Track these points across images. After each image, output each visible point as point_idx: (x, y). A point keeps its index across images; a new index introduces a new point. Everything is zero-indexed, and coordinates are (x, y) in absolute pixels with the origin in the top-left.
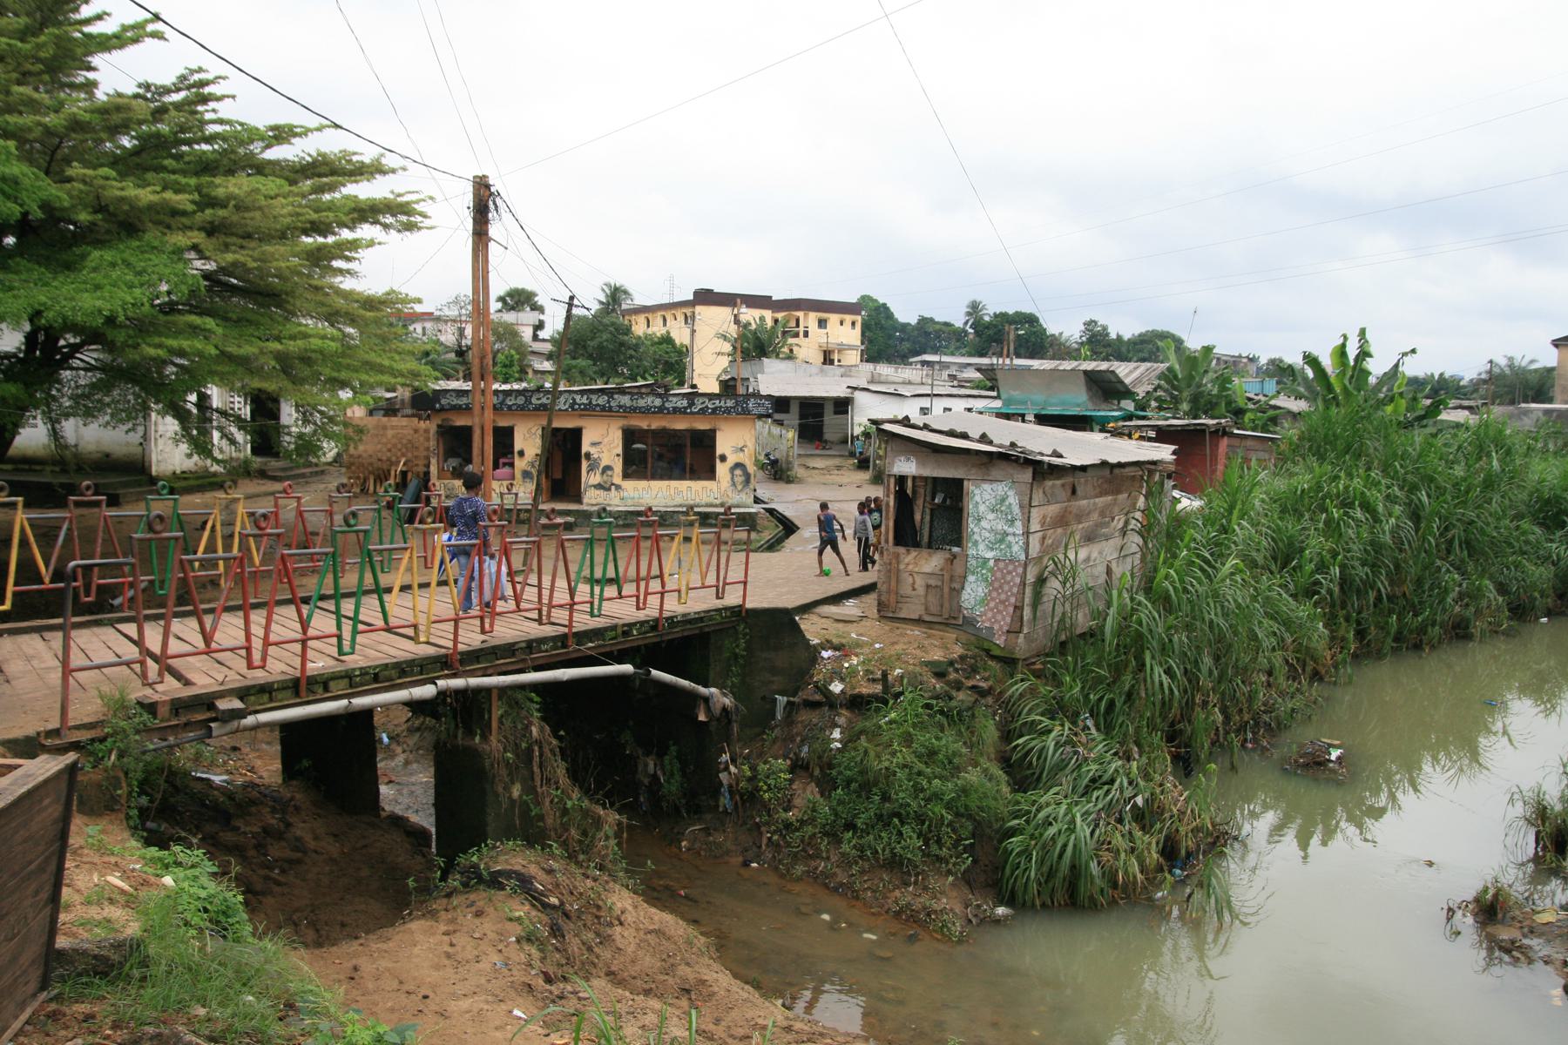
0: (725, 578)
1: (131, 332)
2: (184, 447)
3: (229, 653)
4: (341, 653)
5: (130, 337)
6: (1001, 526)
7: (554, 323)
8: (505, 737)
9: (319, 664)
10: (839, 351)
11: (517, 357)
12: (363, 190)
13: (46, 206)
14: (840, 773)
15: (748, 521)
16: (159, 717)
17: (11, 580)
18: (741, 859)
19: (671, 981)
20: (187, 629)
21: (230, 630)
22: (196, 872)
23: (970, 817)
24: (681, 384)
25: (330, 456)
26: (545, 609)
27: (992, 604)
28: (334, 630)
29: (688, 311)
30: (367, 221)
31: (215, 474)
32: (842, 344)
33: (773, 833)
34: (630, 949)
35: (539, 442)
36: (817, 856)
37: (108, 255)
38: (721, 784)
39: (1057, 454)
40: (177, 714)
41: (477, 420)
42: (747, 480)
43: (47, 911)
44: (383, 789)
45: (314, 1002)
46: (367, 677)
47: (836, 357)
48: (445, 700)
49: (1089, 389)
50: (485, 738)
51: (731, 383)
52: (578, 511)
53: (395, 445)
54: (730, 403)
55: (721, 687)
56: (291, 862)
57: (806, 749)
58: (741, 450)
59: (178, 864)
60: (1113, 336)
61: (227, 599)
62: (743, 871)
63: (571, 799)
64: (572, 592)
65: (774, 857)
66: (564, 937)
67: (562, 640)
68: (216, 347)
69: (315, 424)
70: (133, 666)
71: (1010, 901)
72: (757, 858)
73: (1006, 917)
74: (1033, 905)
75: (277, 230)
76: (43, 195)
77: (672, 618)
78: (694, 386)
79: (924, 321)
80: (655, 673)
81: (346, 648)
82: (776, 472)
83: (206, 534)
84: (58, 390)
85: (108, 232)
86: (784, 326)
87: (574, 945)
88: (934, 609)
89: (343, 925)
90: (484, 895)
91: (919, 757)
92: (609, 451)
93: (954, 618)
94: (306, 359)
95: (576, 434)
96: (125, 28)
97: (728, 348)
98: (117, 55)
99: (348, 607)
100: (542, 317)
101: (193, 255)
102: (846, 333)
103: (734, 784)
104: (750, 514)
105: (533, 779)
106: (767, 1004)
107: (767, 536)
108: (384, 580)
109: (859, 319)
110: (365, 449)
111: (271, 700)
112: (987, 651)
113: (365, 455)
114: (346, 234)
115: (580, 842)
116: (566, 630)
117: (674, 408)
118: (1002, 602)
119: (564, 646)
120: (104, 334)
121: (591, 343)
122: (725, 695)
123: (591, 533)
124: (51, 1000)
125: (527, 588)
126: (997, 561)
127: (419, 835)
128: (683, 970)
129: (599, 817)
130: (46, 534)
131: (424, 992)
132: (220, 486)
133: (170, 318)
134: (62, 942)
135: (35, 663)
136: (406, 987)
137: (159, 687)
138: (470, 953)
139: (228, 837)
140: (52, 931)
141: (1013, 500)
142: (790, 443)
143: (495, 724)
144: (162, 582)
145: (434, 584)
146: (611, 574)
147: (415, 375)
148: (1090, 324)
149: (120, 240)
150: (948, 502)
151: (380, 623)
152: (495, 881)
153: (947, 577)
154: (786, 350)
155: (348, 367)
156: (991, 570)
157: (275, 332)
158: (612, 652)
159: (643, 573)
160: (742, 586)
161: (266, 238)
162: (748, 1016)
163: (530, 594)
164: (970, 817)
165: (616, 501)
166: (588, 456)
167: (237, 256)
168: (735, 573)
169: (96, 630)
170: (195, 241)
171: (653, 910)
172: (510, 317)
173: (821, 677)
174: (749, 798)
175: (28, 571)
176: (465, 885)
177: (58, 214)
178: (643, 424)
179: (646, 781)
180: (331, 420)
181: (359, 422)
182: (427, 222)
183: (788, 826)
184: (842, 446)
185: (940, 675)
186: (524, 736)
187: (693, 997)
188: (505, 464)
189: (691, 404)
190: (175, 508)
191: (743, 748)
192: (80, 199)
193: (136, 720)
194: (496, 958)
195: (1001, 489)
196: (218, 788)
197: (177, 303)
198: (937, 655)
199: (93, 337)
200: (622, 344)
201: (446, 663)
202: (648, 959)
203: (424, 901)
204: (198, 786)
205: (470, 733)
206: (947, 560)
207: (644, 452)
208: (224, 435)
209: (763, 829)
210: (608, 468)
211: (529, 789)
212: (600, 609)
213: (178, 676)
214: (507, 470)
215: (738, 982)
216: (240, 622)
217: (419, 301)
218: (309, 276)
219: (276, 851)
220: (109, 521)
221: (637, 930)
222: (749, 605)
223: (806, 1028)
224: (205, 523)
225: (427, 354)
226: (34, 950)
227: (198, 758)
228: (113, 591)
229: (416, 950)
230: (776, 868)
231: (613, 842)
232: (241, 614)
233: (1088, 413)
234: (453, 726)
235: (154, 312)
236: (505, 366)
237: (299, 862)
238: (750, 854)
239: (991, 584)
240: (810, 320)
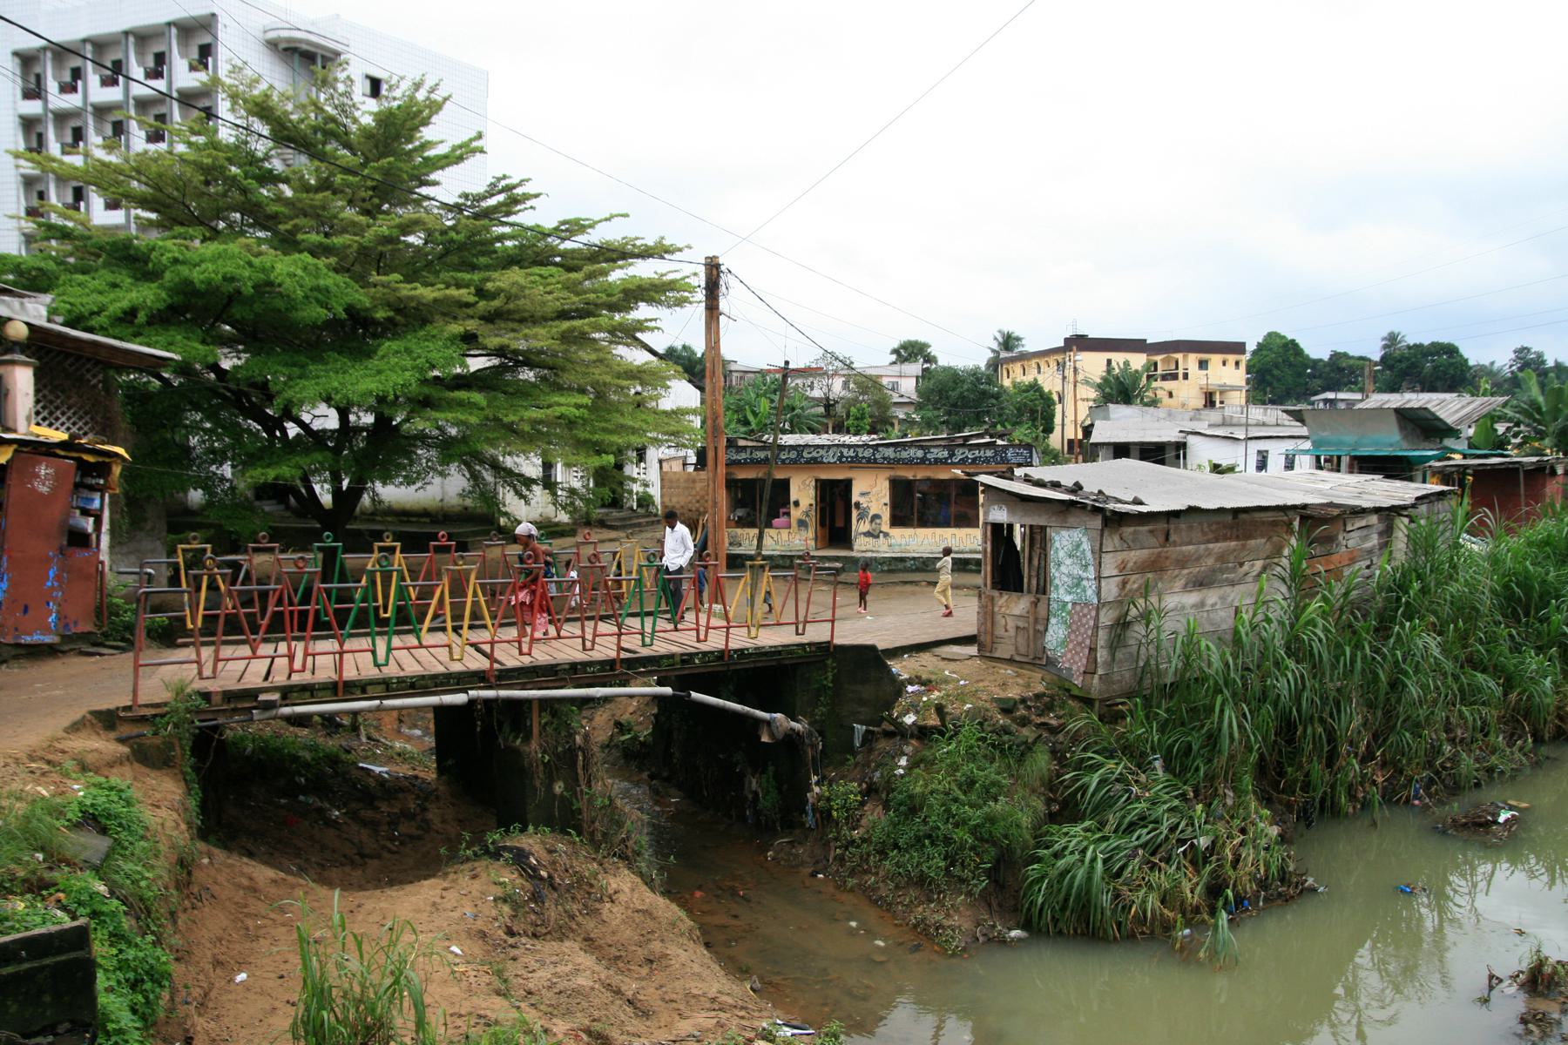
6: (1077, 571)
10: (1222, 393)
12: (644, 270)
13: (349, 309)
17: (202, 606)
23: (994, 843)
27: (1071, 646)
29: (1060, 358)
32: (1225, 385)
35: (812, 492)
39: (1138, 502)
40: (229, 702)
47: (1217, 398)
49: (1402, 428)
50: (527, 739)
52: (845, 557)
56: (412, 837)
57: (878, 774)
60: (1550, 363)
62: (808, 881)
71: (1026, 925)
73: (1020, 940)
74: (1115, 938)
76: (348, 299)
79: (1336, 356)
80: (694, 695)
88: (1023, 650)
91: (960, 786)
95: (847, 485)
96: (454, 149)
98: (450, 170)
102: (1230, 375)
111: (312, 696)
112: (1068, 690)
113: (678, 506)
117: (936, 459)
118: (1079, 644)
126: (1074, 604)
139: (368, 814)
141: (1086, 546)
143: (536, 730)
148: (1522, 352)
154: (1150, 394)
155: (604, 430)
156: (1069, 613)
164: (994, 843)
165: (885, 548)
166: (858, 505)
178: (909, 474)
179: (750, 796)
185: (1007, 711)
188: (784, 514)
189: (952, 455)
195: (1076, 535)
198: (1013, 693)
206: (1032, 603)
210: (876, 517)
216: (370, 641)
219: (405, 828)
222: (837, 641)
233: (1400, 454)
236: (857, 419)
237: (419, 838)
238: (820, 866)
239: (1070, 627)
240: (1192, 360)
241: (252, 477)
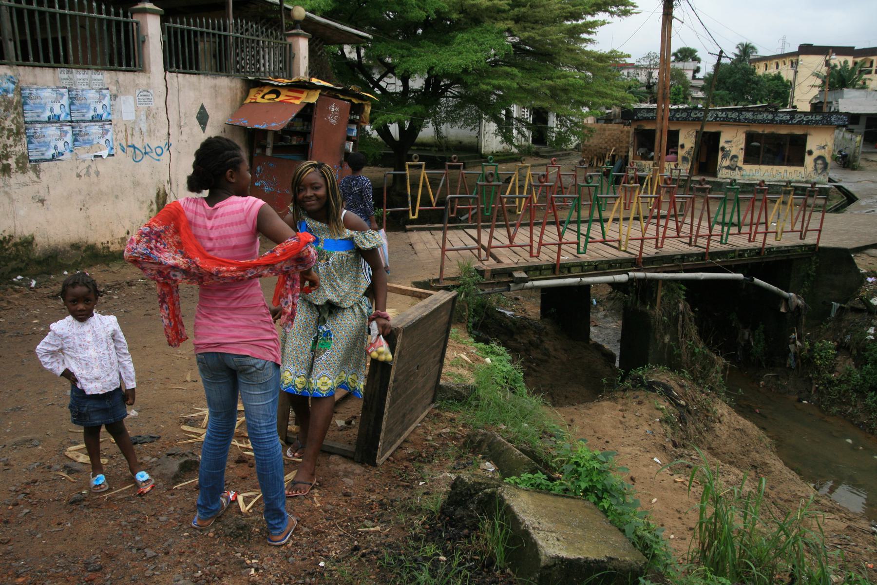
0: (807, 227)
1: (475, 77)
2: (499, 138)
3: (519, 248)
4: (578, 253)
5: (475, 80)
7: (707, 67)
8: (664, 308)
9: (565, 258)
11: (682, 89)
14: (872, 355)
15: (823, 192)
16: (485, 277)
18: (797, 397)
19: (746, 459)
20: (501, 235)
21: (522, 236)
22: (502, 358)
24: (785, 106)
25: (573, 146)
26: (693, 238)
28: (575, 240)
29: (794, 59)
30: (601, 10)
31: (513, 154)
33: (820, 385)
34: (724, 437)
35: (693, 139)
36: (848, 403)
37: (466, 36)
38: (789, 351)
40: (494, 277)
41: (659, 126)
42: (825, 165)
43: (437, 367)
44: (592, 329)
45: (563, 432)
46: (591, 267)
48: (632, 284)
50: (652, 307)
51: (819, 105)
52: (714, 182)
53: (609, 140)
54: (819, 118)
55: (796, 293)
57: (849, 337)
59: (493, 353)
61: (521, 220)
63: (698, 347)
64: (711, 229)
65: (819, 399)
66: (686, 423)
67: (702, 256)
68: (518, 84)
69: (567, 127)
70: (473, 251)
72: (807, 399)
75: (551, 18)
77: (770, 248)
78: (795, 107)
80: (756, 280)
81: (582, 250)
82: (845, 163)
83: (511, 185)
84: (439, 108)
85: (466, 23)
86: (861, 67)
87: (691, 429)
89: (566, 397)
90: (643, 393)
92: (736, 146)
94: (565, 90)
95: (717, 136)
97: (819, 82)
99: (584, 228)
100: (699, 65)
101: (507, 34)
103: (798, 352)
104: (825, 188)
105: (677, 334)
106: (804, 485)
107: (834, 203)
108: (605, 215)
110: (594, 141)
111: (540, 275)
114: (589, 18)
115: (701, 372)
116: (705, 250)
117: (781, 121)
119: (703, 260)
120: (462, 79)
122: (799, 298)
123: (726, 194)
124: (436, 408)
125: (684, 225)
127: (610, 357)
128: (754, 455)
129: (714, 360)
130: (434, 182)
131: (606, 439)
132: (516, 160)
133: (494, 68)
134: (442, 382)
135: (428, 245)
136: (597, 435)
137: (486, 263)
138: (633, 423)
139: (512, 343)
140: (439, 377)
142: (857, 144)
143: (658, 300)
144: (487, 209)
145: (631, 218)
146: (735, 219)
147: (623, 99)
149: (472, 27)
151: (600, 238)
152: (650, 387)
154: (860, 83)
155: (587, 94)
157: (549, 75)
158: (731, 266)
159: (755, 221)
160: (817, 233)
161: (545, 22)
162: (793, 488)
163: (686, 229)
166: (723, 149)
167: (530, 34)
168: (814, 224)
169: (456, 231)
170: (509, 26)
171: (740, 418)
172: (679, 65)
173: (865, 293)
174: (807, 362)
175: (426, 201)
176: (634, 386)
177: (442, 15)
178: (759, 130)
179: (743, 343)
180: (576, 124)
181: (590, 126)
182: (636, 10)
183: (830, 382)
186: (675, 308)
187: (759, 471)
188: (672, 153)
189: (792, 118)
190: (496, 170)
191: (807, 331)
192: (453, 7)
193: (475, 278)
194: (647, 428)
196: (508, 318)
197: (499, 61)
199: (456, 79)
200: (749, 80)
201: (635, 263)
202: (733, 444)
203: (611, 392)
204: (499, 316)
205: (644, 303)
207: (758, 148)
208: (519, 132)
209: (814, 381)
210: (735, 157)
211: (674, 338)
212: (726, 240)
213: (495, 258)
214: (673, 156)
215: (787, 468)
217: (629, 56)
218: (568, 44)
219: (535, 354)
220: (464, 175)
221: (729, 427)
222: (821, 245)
223: (828, 504)
224: (510, 178)
225: (630, 88)
226: (431, 384)
227: (498, 302)
228: (461, 212)
229: (604, 417)
230: (820, 406)
231: (720, 375)
232: (528, 228)
234: (635, 298)
235: (487, 65)
236: (675, 94)
237: (546, 361)
241: (381, 120)
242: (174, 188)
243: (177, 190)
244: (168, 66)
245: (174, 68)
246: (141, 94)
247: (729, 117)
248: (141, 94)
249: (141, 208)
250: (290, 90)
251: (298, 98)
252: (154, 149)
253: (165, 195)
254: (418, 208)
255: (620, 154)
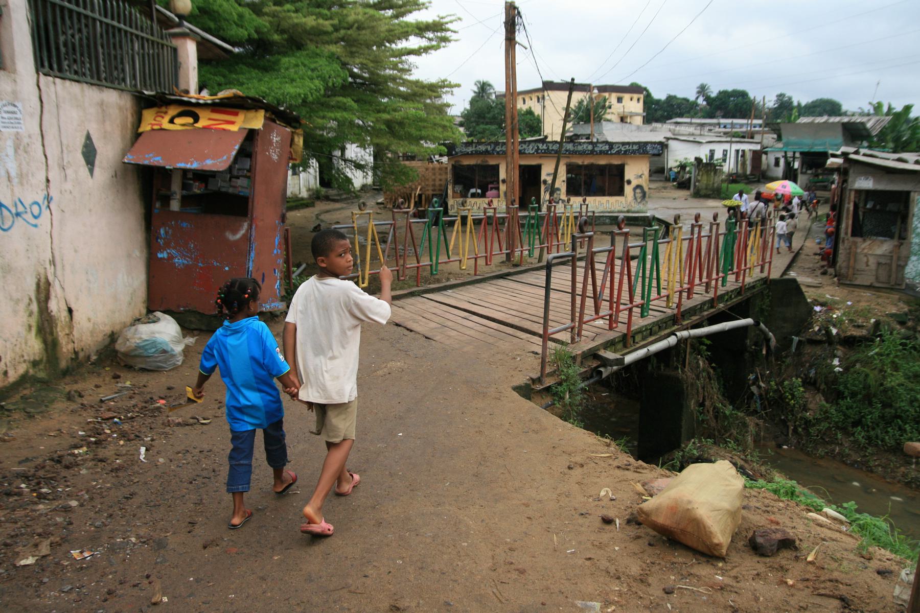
29: (540, 95)
32: (631, 112)
36: (834, 441)
37: (293, 60)
49: (844, 135)
58: (641, 176)
60: (795, 104)
65: (799, 442)
76: (255, 24)
79: (670, 98)
93: (899, 285)
102: (634, 105)
103: (764, 393)
109: (642, 96)
119: (712, 307)
121: (488, 116)
148: (780, 96)
150: (878, 207)
153: (895, 258)
178: (580, 161)
184: (660, 175)
240: (613, 98)
242: (59, 272)
243: (63, 275)
244: (40, 65)
245: (47, 69)
246: (6, 109)
247: (550, 148)
248: (6, 109)
249: (15, 312)
250: (213, 111)
251: (232, 123)
252: (28, 207)
253: (48, 284)
254: (367, 272)
255: (427, 193)
